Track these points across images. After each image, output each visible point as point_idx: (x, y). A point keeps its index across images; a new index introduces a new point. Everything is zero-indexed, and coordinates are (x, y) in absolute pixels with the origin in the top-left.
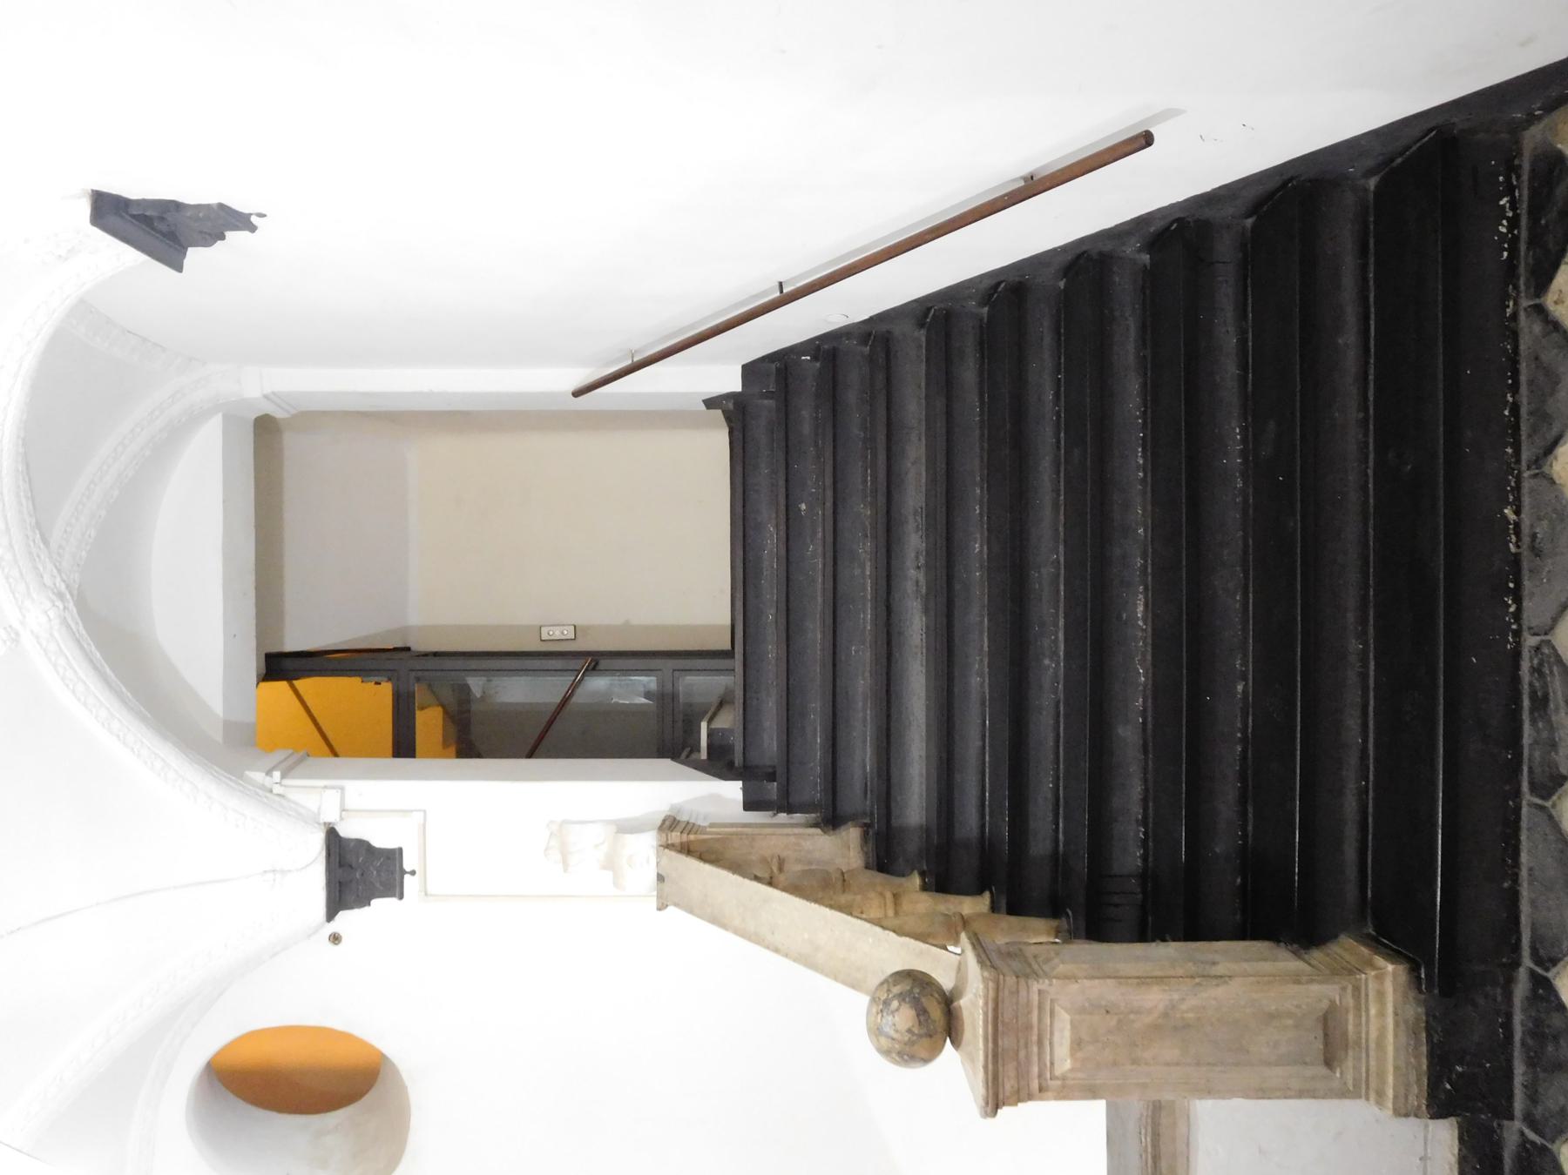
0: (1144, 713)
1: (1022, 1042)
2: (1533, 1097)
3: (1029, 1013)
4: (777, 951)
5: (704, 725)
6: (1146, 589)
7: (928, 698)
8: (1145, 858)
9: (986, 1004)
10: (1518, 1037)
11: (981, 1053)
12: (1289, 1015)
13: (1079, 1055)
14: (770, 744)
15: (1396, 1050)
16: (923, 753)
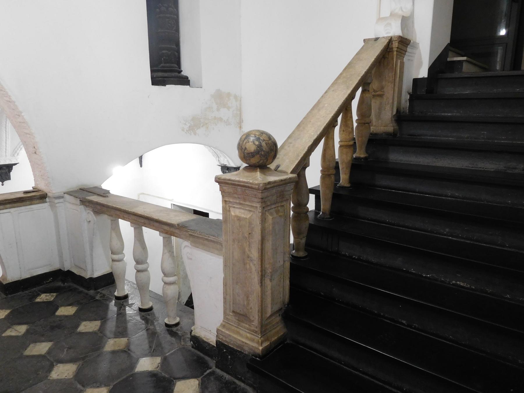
0: (407, 272)
1: (240, 196)
2: (219, 378)
3: (250, 202)
4: (326, 92)
5: (465, 58)
6: (472, 289)
7: (449, 168)
8: (345, 255)
9: (251, 183)
10: (237, 382)
11: (237, 179)
12: (248, 304)
13: (236, 219)
14: (450, 91)
15: (235, 338)
16: (421, 163)
